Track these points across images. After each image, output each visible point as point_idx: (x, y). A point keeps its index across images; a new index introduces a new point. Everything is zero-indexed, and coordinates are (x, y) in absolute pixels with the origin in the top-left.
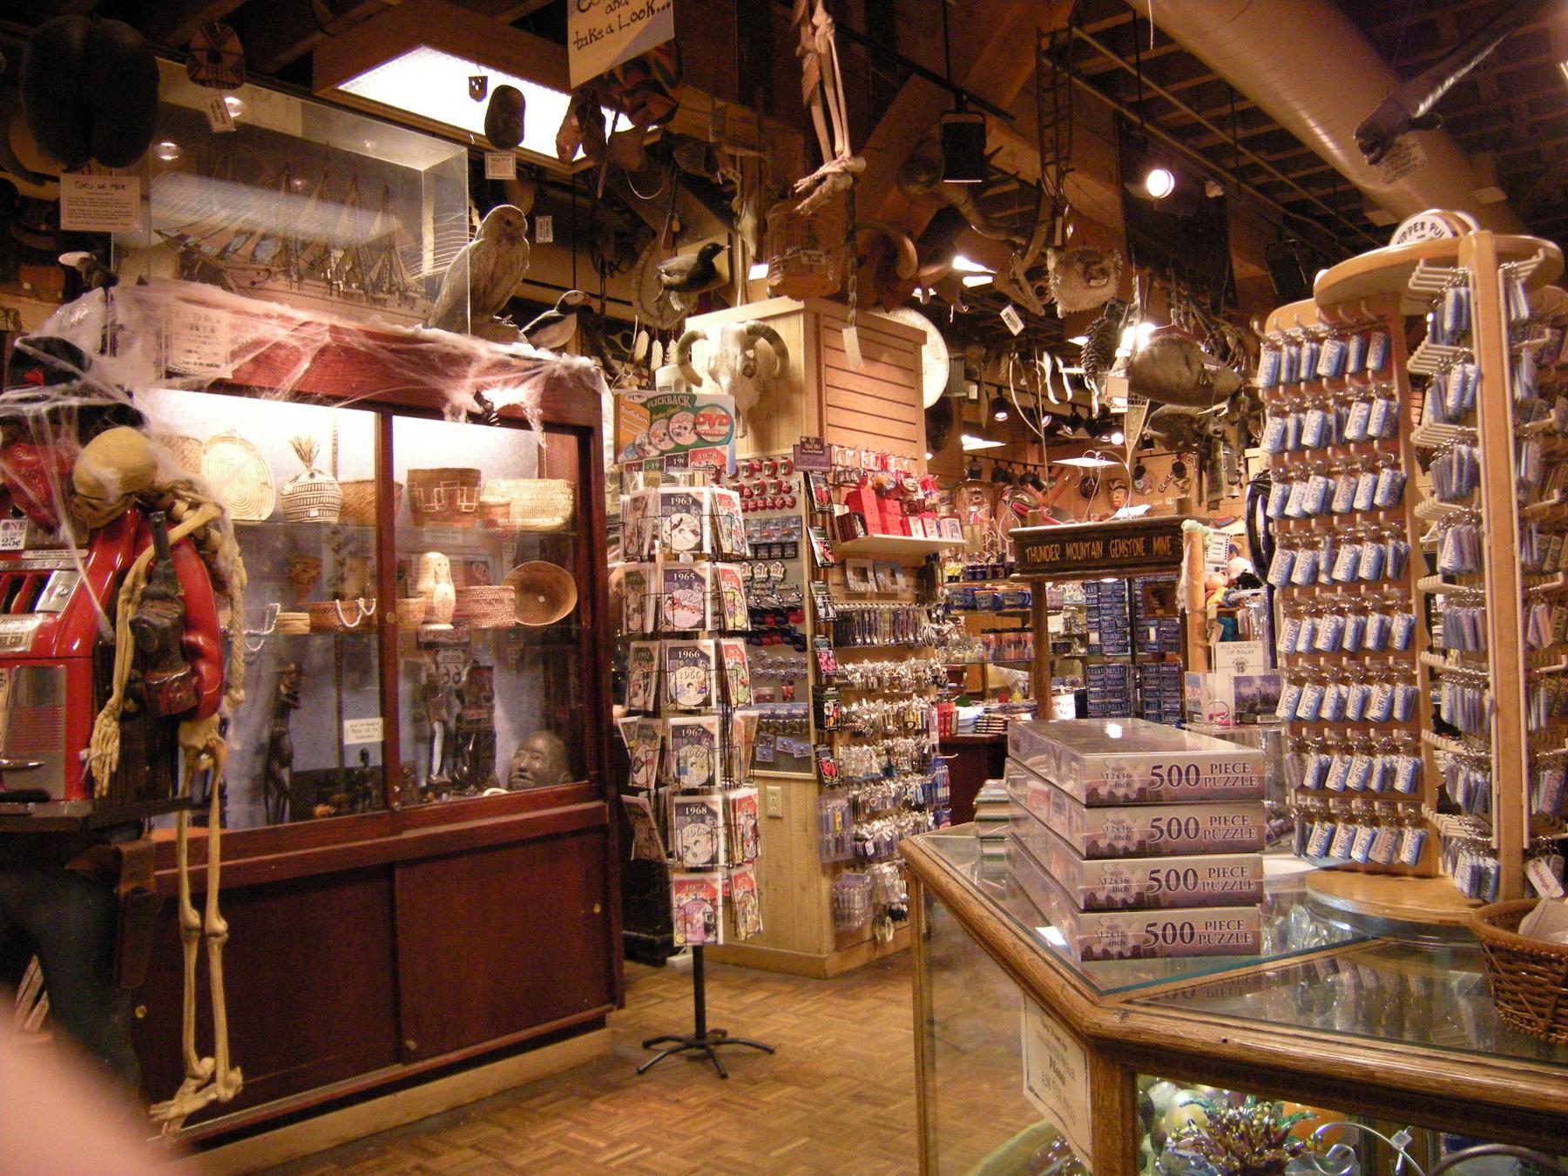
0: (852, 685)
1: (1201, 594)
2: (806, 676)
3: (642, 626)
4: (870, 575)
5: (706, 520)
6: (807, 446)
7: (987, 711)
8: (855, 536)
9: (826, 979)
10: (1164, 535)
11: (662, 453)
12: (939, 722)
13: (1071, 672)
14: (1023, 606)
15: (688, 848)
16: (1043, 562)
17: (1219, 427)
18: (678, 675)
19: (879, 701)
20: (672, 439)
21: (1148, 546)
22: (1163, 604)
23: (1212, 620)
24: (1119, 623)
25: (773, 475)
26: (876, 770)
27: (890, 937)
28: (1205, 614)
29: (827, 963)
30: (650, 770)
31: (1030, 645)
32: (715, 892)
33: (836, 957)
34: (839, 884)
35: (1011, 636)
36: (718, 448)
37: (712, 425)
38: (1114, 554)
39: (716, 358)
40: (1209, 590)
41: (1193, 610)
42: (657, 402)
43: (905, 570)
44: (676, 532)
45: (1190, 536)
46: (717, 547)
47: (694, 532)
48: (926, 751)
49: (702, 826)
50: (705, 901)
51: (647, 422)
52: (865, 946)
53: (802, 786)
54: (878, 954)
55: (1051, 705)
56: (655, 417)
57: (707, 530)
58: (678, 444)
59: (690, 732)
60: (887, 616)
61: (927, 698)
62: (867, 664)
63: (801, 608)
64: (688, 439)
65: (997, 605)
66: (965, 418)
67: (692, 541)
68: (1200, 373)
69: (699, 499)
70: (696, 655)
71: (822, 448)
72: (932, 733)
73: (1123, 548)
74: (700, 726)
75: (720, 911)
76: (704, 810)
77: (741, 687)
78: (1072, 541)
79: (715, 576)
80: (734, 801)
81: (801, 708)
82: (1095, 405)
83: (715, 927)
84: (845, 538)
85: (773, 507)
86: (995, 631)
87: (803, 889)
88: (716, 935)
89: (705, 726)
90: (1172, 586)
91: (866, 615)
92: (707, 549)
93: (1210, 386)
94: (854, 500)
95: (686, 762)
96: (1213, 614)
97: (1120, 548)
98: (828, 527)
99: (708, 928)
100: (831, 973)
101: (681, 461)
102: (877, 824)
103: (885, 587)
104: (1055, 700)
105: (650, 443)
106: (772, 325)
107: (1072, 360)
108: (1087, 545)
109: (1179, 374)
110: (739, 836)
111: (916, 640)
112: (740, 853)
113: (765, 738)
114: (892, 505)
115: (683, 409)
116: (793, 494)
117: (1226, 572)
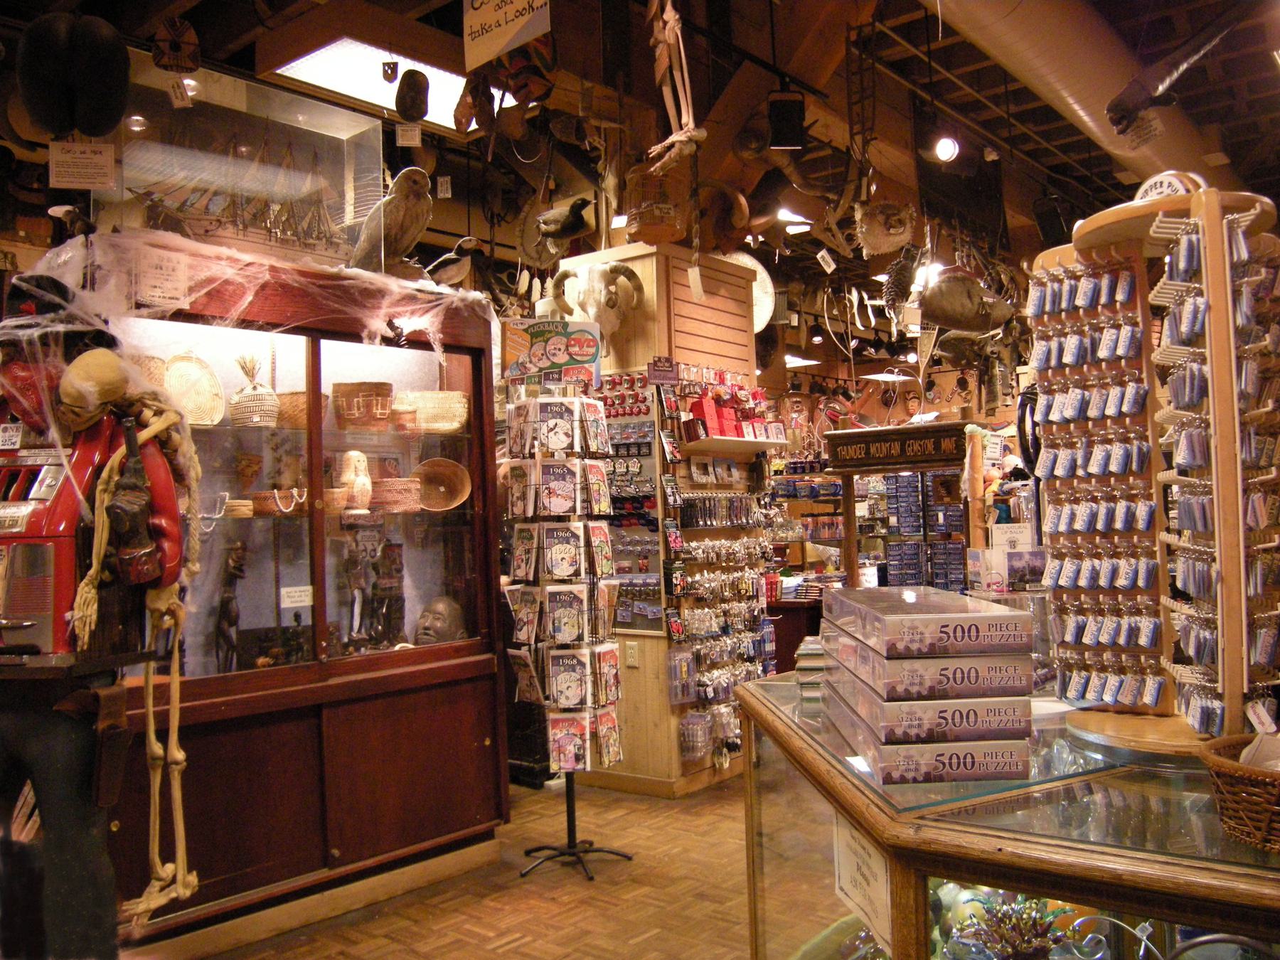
0: (696, 559)
1: (981, 485)
2: (658, 551)
3: (524, 511)
4: (710, 469)
5: (577, 424)
6: (659, 364)
7: (806, 580)
8: (698, 438)
9: (674, 799)
10: (950, 437)
11: (541, 370)
12: (767, 589)
13: (875, 548)
14: (835, 494)
15: (561, 692)
16: (852, 459)
17: (995, 349)
18: (554, 551)
19: (718, 572)
20: (548, 358)
21: (937, 446)
22: (949, 493)
23: (990, 506)
24: (914, 509)
25: (631, 388)
26: (715, 628)
27: (726, 765)
28: (984, 501)
29: (675, 786)
30: (530, 629)
31: (841, 527)
32: (583, 728)
33: (682, 781)
34: (685, 721)
35: (826, 519)
36: (586, 365)
37: (581, 347)
38: (909, 452)
39: (584, 292)
40: (987, 482)
41: (974, 498)
42: (536, 329)
43: (739, 465)
44: (551, 434)
45: (972, 437)
46: (586, 446)
47: (567, 434)
48: (756, 613)
49: (573, 674)
50: (576, 735)
51: (528, 345)
52: (706, 772)
53: (655, 642)
54: (717, 779)
55: (858, 576)
56: (534, 340)
57: (577, 432)
58: (553, 363)
59: (563, 597)
60: (724, 502)
61: (756, 570)
62: (708, 542)
63: (654, 496)
64: (562, 358)
65: (814, 494)
66: (788, 341)
67: (565, 442)
68: (979, 304)
69: (571, 407)
70: (568, 534)
71: (671, 366)
72: (760, 599)
73: (916, 447)
74: (571, 593)
75: (588, 744)
76: (575, 661)
77: (605, 561)
78: (875, 442)
79: (584, 470)
80: (599, 654)
81: (654, 578)
82: (894, 330)
83: (584, 757)
84: (690, 439)
85: (631, 414)
86: (812, 515)
87: (656, 725)
88: (585, 763)
89: (576, 593)
90: (957, 478)
91: (707, 502)
92: (577, 448)
93: (988, 315)
94: (697, 408)
95: (560, 622)
96: (990, 501)
97: (914, 447)
98: (676, 430)
99: (578, 758)
100: (678, 795)
101: (556, 376)
102: (716, 673)
103: (722, 479)
104: (861, 571)
105: (531, 362)
106: (630, 265)
107: (875, 294)
108: (888, 445)
109: (963, 305)
110: (604, 683)
111: (748, 523)
112: (604, 697)
113: (624, 602)
114: (728, 412)
115: (557, 334)
116: (647, 403)
117: (1001, 467)
